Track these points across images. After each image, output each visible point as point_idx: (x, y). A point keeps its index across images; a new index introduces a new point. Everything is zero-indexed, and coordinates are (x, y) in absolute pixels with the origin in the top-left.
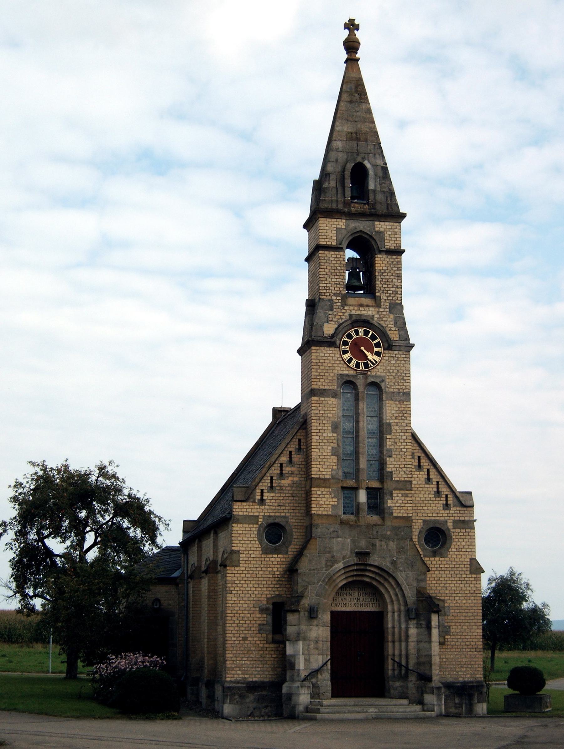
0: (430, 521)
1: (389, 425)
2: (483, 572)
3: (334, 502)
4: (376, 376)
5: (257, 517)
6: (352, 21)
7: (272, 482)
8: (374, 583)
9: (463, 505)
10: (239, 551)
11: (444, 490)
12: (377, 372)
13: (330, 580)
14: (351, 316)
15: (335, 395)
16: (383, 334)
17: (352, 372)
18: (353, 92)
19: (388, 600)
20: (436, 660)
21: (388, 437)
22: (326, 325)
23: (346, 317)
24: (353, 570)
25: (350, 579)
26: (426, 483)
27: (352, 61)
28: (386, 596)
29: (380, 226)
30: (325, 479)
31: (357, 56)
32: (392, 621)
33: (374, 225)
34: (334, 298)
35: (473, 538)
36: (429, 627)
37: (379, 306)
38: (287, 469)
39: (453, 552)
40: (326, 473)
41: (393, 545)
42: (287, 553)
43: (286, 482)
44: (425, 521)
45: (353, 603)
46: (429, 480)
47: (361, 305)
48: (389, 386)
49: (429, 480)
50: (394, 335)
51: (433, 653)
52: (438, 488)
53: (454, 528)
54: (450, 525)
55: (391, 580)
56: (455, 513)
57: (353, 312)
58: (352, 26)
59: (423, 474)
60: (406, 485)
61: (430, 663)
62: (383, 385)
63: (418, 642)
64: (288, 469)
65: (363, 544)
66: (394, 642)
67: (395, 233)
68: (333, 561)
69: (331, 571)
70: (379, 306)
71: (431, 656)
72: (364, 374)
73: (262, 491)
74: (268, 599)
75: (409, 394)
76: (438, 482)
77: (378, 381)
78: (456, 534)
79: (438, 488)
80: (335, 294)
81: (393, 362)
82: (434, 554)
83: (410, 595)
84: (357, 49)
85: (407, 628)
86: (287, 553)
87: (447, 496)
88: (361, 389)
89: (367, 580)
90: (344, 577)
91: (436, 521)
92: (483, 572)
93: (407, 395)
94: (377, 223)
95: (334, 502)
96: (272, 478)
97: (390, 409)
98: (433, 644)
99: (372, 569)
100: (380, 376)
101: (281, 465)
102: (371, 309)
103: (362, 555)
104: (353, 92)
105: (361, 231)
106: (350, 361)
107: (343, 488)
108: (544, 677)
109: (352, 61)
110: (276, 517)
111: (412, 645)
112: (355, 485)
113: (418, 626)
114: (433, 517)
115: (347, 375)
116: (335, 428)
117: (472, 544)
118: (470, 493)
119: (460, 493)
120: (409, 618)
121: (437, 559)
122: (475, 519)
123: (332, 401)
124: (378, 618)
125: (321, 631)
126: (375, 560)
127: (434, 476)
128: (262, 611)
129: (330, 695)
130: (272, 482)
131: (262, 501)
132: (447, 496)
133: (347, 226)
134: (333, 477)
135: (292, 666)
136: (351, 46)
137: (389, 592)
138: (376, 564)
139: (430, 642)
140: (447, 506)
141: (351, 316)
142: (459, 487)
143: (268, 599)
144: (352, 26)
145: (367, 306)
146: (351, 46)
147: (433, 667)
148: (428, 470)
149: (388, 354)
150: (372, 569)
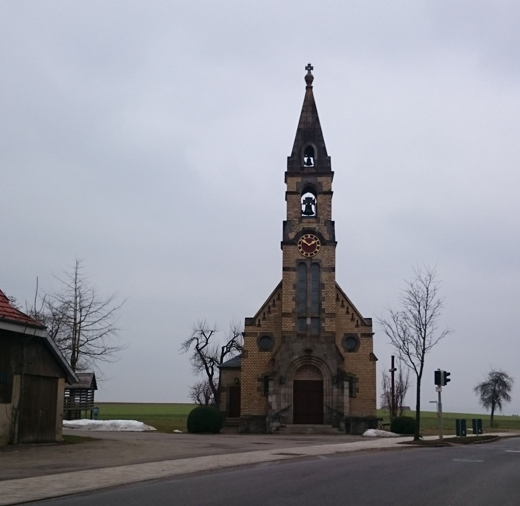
0: (348, 334)
1: (324, 284)
2: (377, 360)
3: (293, 324)
4: (317, 260)
5: (257, 333)
6: (309, 65)
7: (264, 316)
8: (316, 366)
9: (366, 325)
10: (247, 351)
11: (356, 318)
12: (317, 257)
13: (292, 364)
14: (303, 228)
15: (294, 270)
16: (320, 236)
17: (304, 258)
18: (310, 107)
19: (324, 374)
20: (347, 405)
21: (323, 291)
22: (290, 234)
23: (301, 229)
24: (304, 359)
25: (304, 364)
26: (346, 314)
27: (309, 88)
28: (323, 372)
29: (320, 179)
30: (289, 313)
31: (312, 85)
32: (326, 386)
33: (317, 179)
34: (295, 219)
35: (372, 342)
36: (343, 388)
37: (319, 222)
38: (272, 309)
39: (360, 349)
40: (290, 310)
41: (325, 346)
42: (272, 351)
43: (271, 315)
44: (345, 334)
45: (307, 376)
46: (348, 313)
47: (309, 223)
48: (325, 264)
49: (348, 313)
50: (327, 237)
51: (345, 401)
52: (353, 316)
53: (361, 337)
54: (359, 335)
55: (324, 364)
56: (363, 330)
57: (305, 226)
58: (309, 68)
59: (345, 310)
60: (333, 315)
61: (343, 407)
62: (320, 264)
63: (338, 396)
64: (273, 309)
65: (309, 346)
66: (326, 396)
67: (328, 183)
68: (293, 354)
69: (292, 360)
70: (319, 222)
71: (343, 403)
72: (310, 258)
73: (259, 320)
74: (262, 374)
75: (334, 268)
76: (353, 314)
77: (318, 262)
78: (363, 341)
79: (353, 316)
80: (295, 218)
81: (326, 251)
82: (350, 351)
83: (334, 371)
84: (312, 81)
85: (332, 389)
86: (272, 351)
87: (357, 320)
88: (309, 266)
89: (313, 364)
90: (300, 363)
91: (352, 334)
92: (377, 360)
93: (333, 269)
94: (318, 178)
95: (293, 324)
96: (264, 313)
97: (324, 276)
98: (345, 397)
99: (314, 358)
100: (319, 260)
101: (269, 306)
102: (314, 224)
103: (308, 351)
104: (310, 107)
105: (309, 183)
106: (302, 252)
107: (299, 318)
108: (511, 415)
109: (309, 88)
110: (266, 333)
111: (335, 397)
112: (305, 316)
113: (338, 387)
114: (349, 331)
115: (301, 260)
116: (295, 287)
117: (371, 345)
118: (371, 319)
119: (365, 319)
120: (333, 384)
121: (352, 353)
122: (373, 332)
123: (294, 273)
124: (321, 383)
125: (288, 390)
126: (315, 354)
127: (350, 310)
128: (259, 380)
129: (292, 421)
130: (264, 316)
131: (259, 325)
132: (357, 320)
133: (302, 180)
134: (293, 312)
135: (270, 407)
136: (309, 79)
137: (324, 370)
138: (315, 356)
139: (343, 396)
140: (357, 326)
141: (303, 228)
142: (364, 316)
143: (262, 374)
144: (309, 68)
145: (313, 223)
146: (309, 79)
147: (345, 409)
148: (347, 307)
149: (323, 247)
150: (314, 358)
